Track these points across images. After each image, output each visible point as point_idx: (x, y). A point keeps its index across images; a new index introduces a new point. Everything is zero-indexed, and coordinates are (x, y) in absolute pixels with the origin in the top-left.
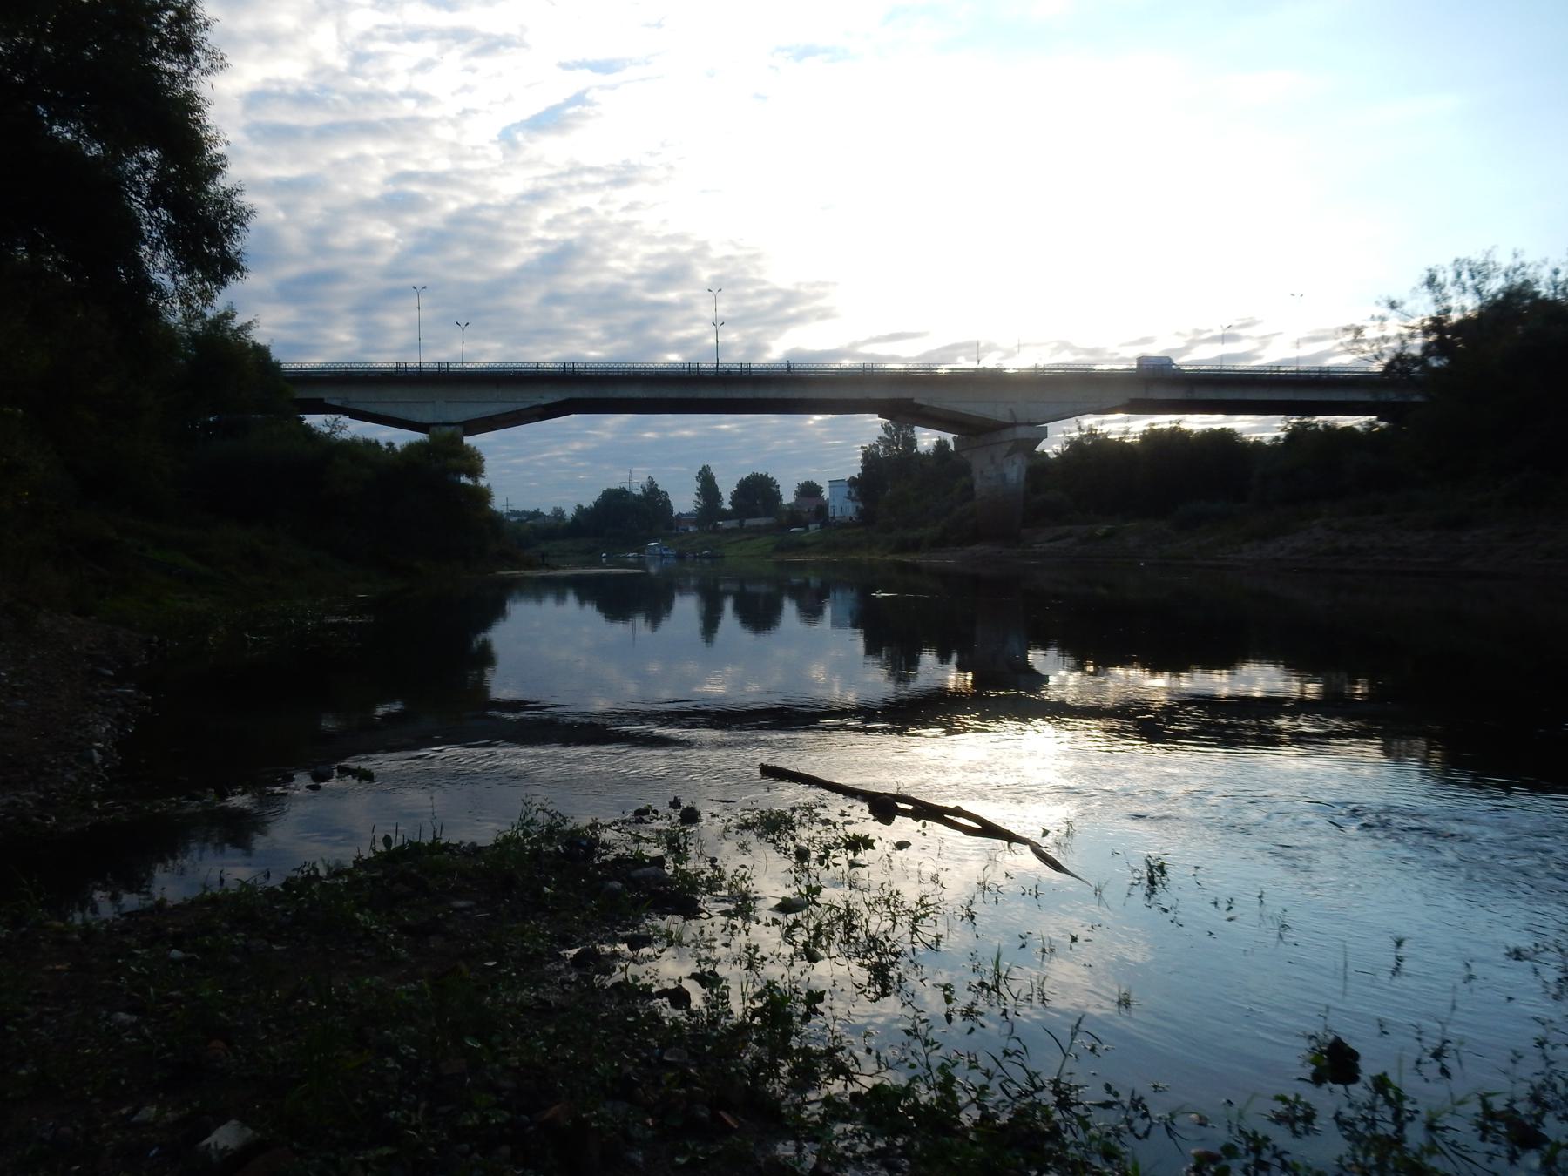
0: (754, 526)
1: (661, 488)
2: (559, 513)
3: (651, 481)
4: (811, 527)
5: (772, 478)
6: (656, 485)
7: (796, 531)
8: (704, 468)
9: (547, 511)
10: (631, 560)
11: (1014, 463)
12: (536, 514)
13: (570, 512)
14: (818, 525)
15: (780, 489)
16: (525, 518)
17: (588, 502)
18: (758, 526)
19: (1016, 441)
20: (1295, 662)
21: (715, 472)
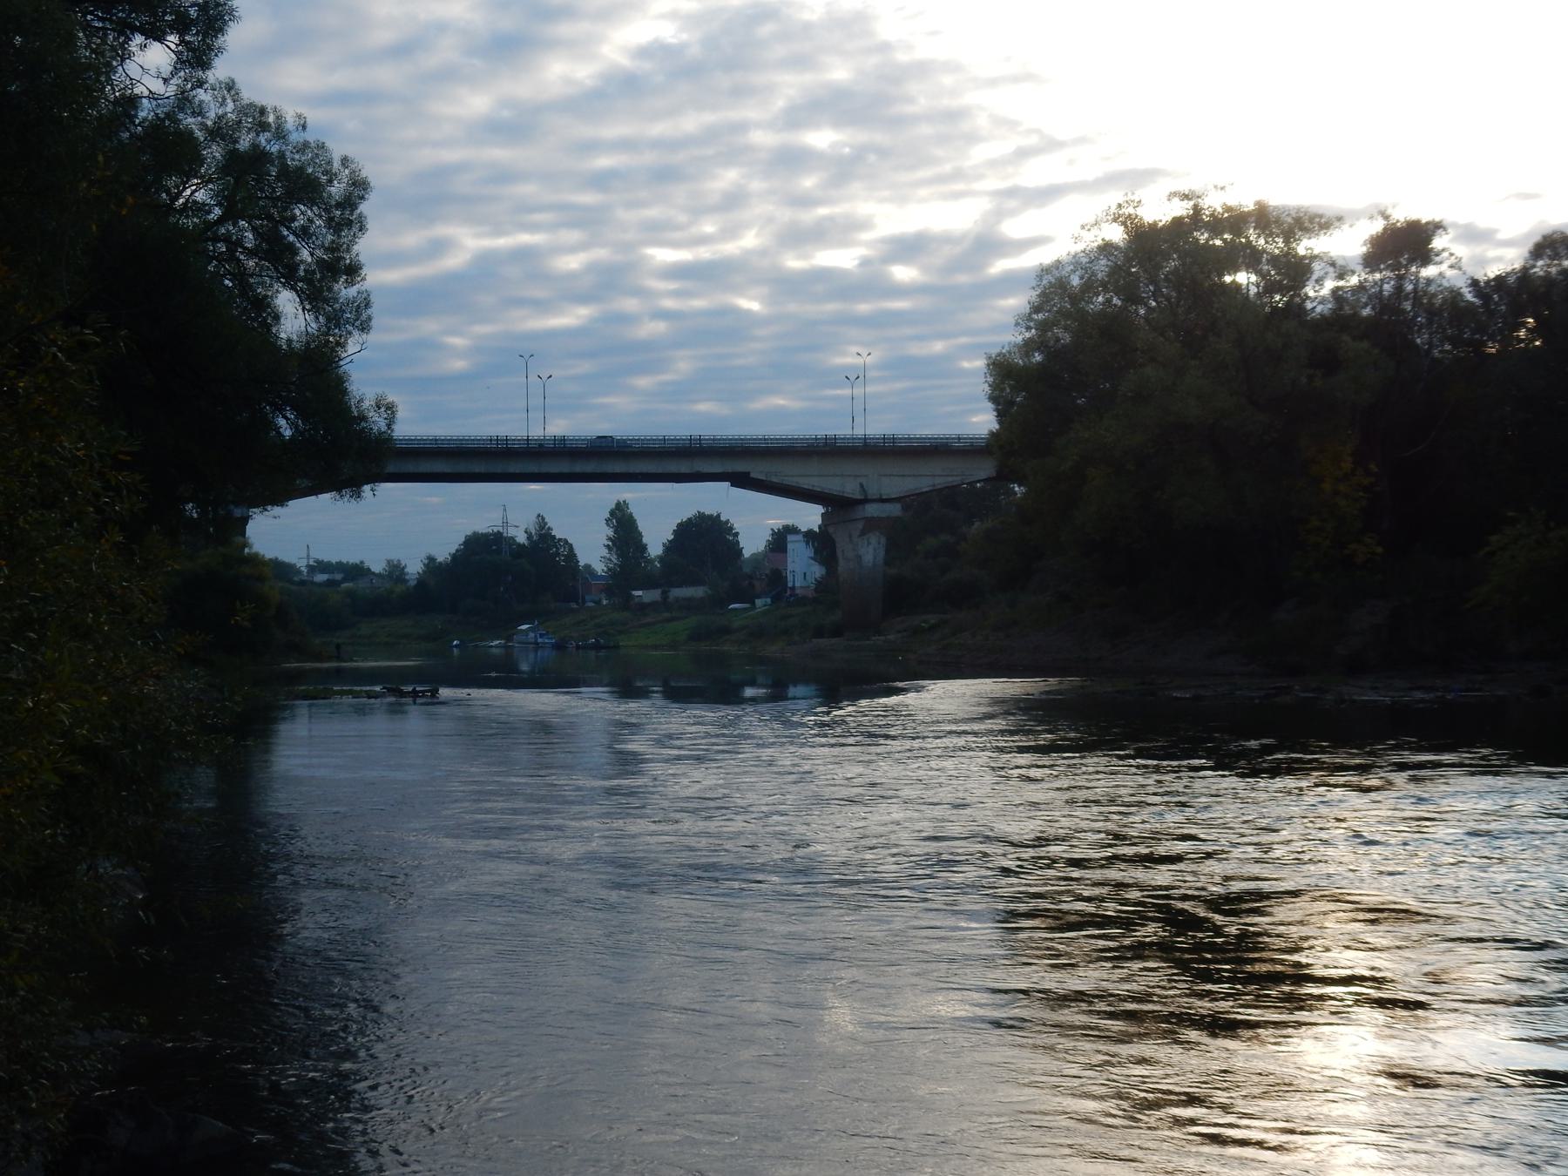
0: (684, 599)
1: (558, 533)
2: (396, 572)
3: (541, 522)
4: (759, 602)
5: (728, 521)
6: (549, 528)
7: (736, 609)
8: (618, 504)
9: (377, 567)
10: (494, 650)
11: (869, 544)
12: (356, 571)
13: (414, 568)
14: (769, 600)
15: (740, 538)
16: (338, 577)
17: (443, 554)
18: (690, 599)
19: (866, 519)
20: (1208, 758)
21: (634, 510)
